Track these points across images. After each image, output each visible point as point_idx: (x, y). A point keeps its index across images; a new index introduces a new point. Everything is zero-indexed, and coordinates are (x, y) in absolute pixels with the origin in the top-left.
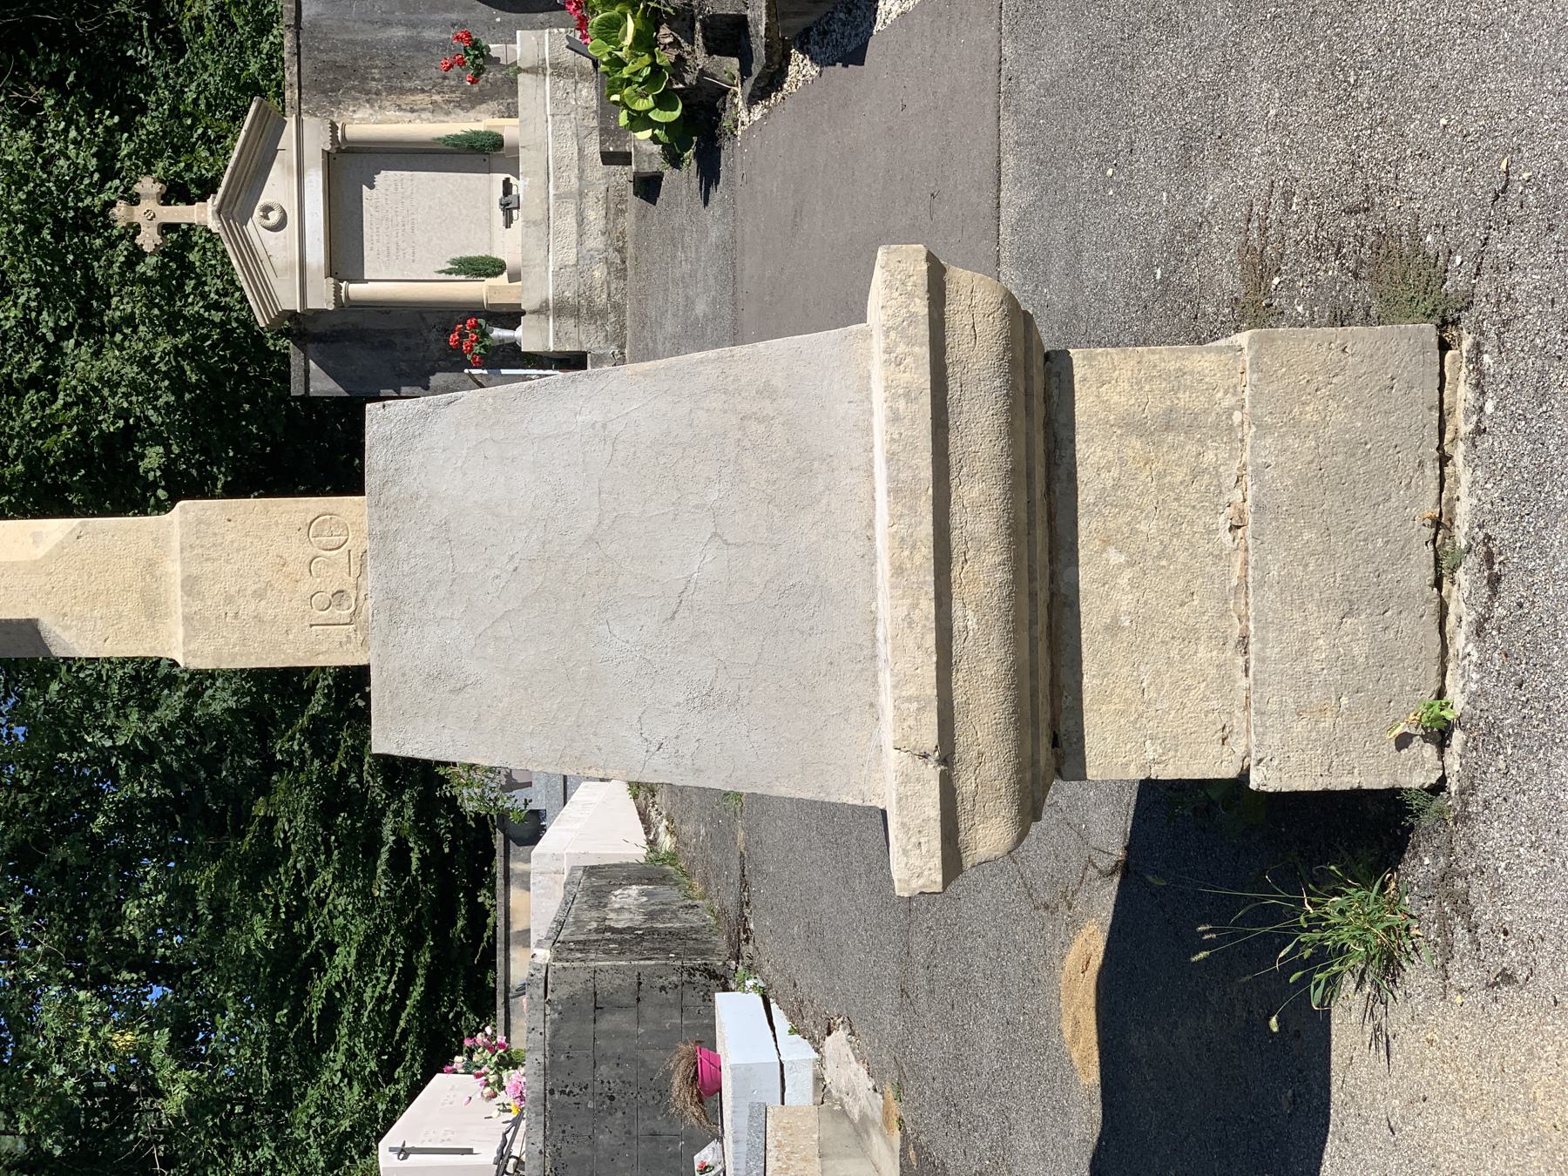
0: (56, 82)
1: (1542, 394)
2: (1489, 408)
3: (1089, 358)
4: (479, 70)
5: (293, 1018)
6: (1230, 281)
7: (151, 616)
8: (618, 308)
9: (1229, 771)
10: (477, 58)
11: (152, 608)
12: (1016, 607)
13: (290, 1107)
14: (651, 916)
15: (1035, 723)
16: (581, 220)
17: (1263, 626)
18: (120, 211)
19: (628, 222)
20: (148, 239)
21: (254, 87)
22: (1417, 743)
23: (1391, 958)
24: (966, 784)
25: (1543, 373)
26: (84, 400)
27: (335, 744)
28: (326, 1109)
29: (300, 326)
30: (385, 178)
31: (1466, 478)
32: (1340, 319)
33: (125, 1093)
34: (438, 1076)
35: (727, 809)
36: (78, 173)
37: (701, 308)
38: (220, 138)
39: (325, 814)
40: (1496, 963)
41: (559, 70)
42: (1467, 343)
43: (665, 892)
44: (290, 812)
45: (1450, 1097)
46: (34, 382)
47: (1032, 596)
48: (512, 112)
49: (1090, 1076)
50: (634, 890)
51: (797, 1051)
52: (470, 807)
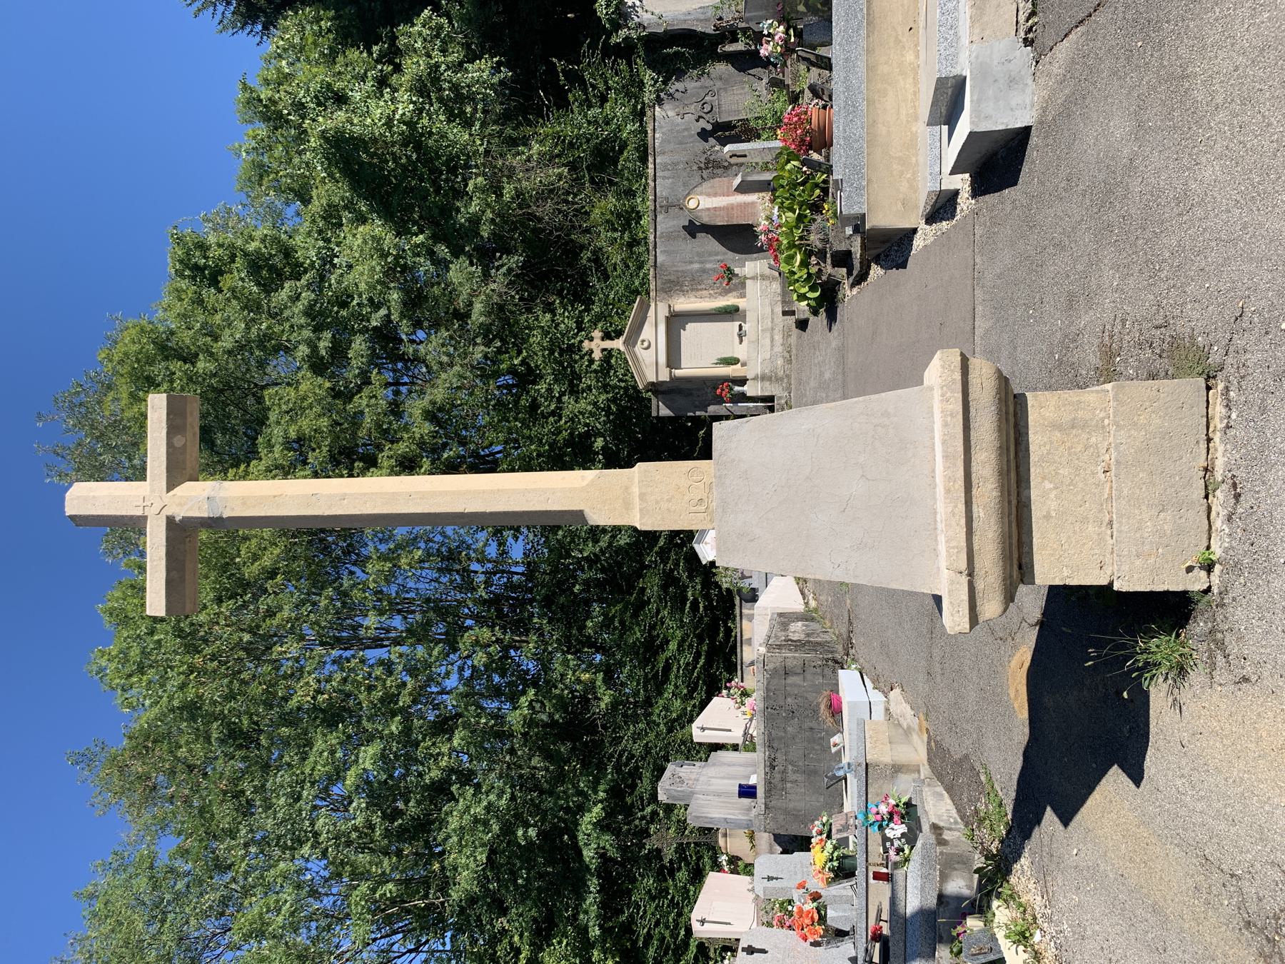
0: (560, 294)
1: (1263, 410)
2: (1234, 416)
3: (1035, 397)
4: (730, 279)
5: (652, 669)
6: (1094, 359)
7: (627, 509)
8: (788, 377)
9: (1104, 582)
10: (729, 274)
11: (627, 506)
12: (1002, 507)
13: (651, 705)
14: (808, 635)
15: (1011, 559)
16: (772, 340)
17: (1120, 516)
18: (586, 344)
19: (793, 340)
20: (597, 355)
21: (637, 292)
22: (1196, 570)
23: (1182, 668)
24: (980, 585)
25: (1263, 400)
26: (572, 420)
27: (668, 558)
28: (666, 708)
29: (656, 388)
30: (690, 326)
31: (1221, 448)
32: (1152, 376)
33: (586, 697)
34: (715, 699)
35: (841, 589)
36: (569, 330)
37: (827, 375)
38: (624, 312)
39: (664, 587)
40: (1240, 673)
41: (764, 277)
42: (1221, 386)
43: (814, 626)
44: (651, 585)
45: (1214, 733)
46: (553, 413)
47: (1009, 502)
48: (743, 296)
49: (1024, 714)
50: (800, 624)
51: (877, 697)
52: (725, 586)
